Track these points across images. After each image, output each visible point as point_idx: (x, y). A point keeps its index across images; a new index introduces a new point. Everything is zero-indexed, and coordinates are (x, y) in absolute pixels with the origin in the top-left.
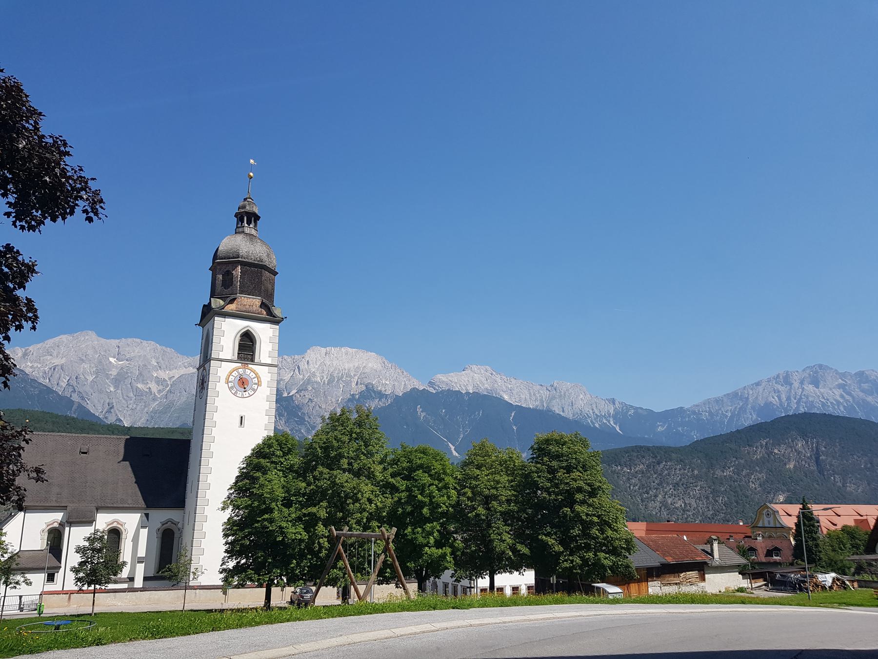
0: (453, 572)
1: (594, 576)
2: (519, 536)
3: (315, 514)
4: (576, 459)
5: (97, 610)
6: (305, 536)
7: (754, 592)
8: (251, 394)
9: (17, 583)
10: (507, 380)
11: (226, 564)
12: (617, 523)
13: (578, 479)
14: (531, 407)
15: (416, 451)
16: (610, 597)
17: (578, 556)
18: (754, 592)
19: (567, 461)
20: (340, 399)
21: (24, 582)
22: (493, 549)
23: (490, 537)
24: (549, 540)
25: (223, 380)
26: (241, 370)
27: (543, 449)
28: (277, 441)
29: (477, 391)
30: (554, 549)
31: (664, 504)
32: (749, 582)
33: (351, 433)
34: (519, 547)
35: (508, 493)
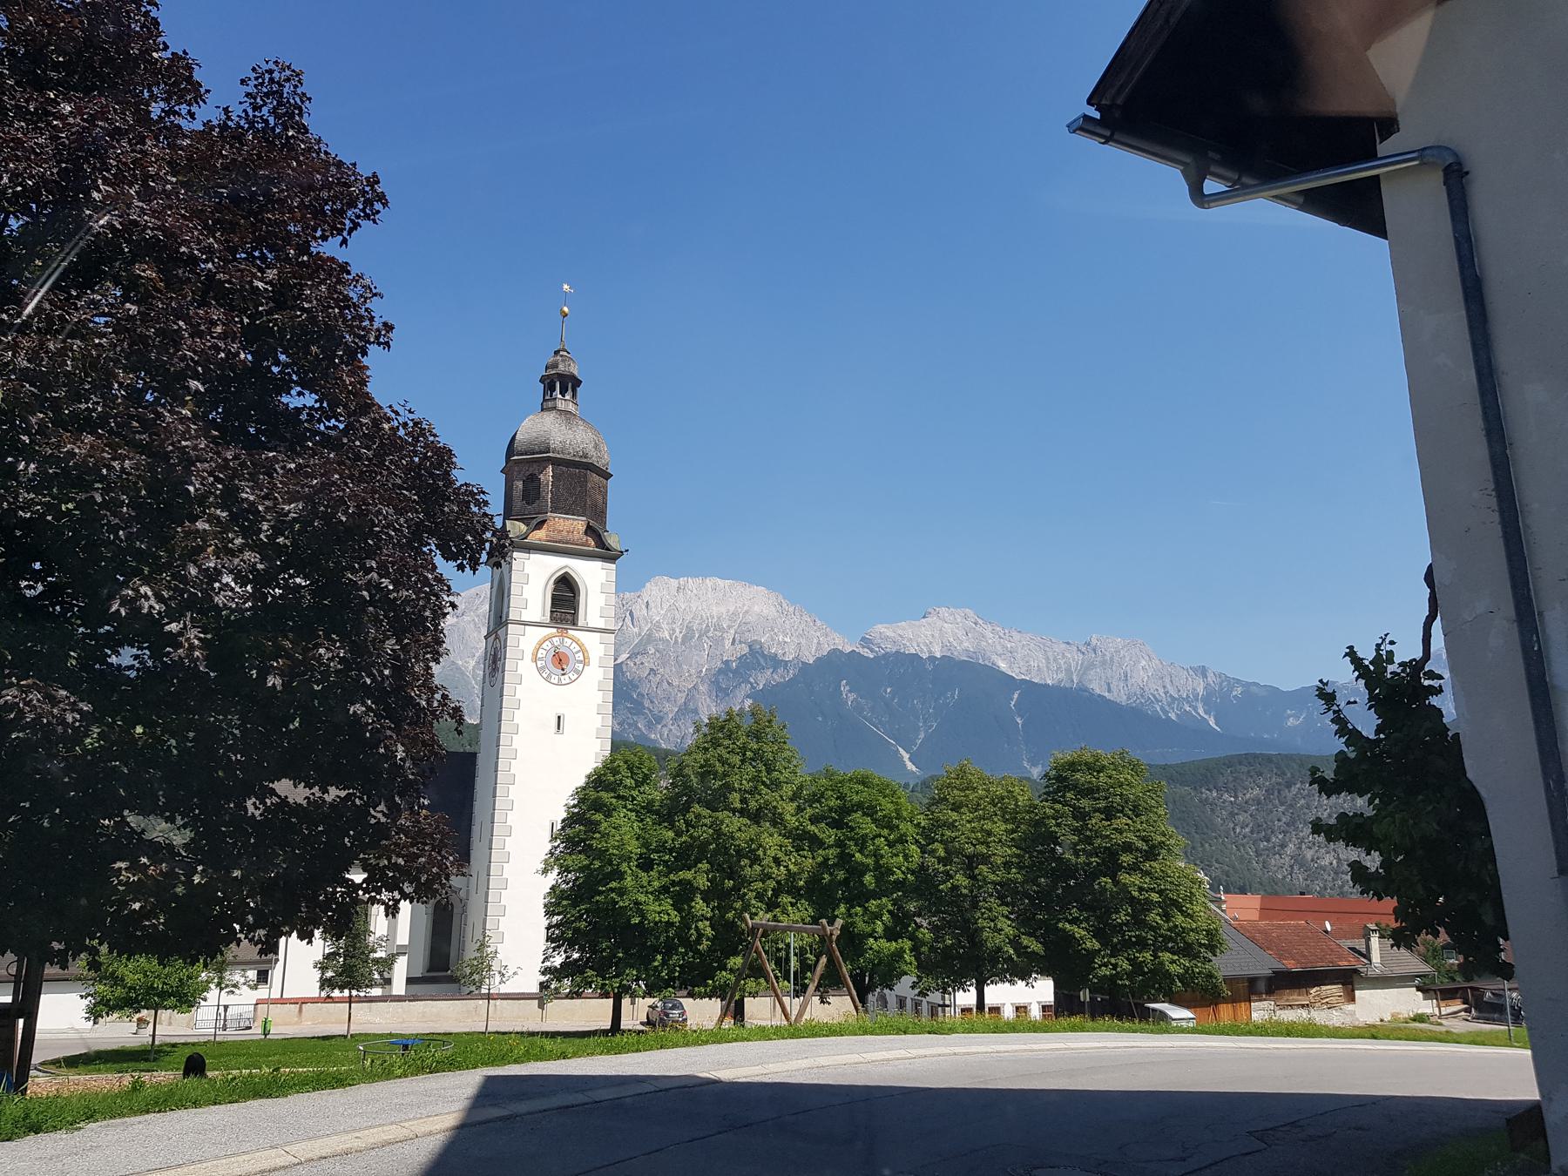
0: (915, 979)
1: (1153, 992)
2: (1025, 922)
3: (689, 882)
4: (1121, 795)
5: (354, 1029)
6: (675, 917)
7: (1443, 1022)
8: (573, 678)
9: (235, 986)
10: (1005, 634)
11: (551, 959)
12: (1192, 904)
13: (1124, 829)
14: (1050, 682)
15: (851, 780)
16: (1174, 1024)
17: (1125, 957)
18: (1443, 1022)
19: (1106, 798)
20: (704, 670)
21: (244, 984)
22: (982, 943)
23: (976, 923)
24: (1076, 930)
25: (528, 656)
26: (557, 639)
27: (1066, 779)
28: (626, 762)
29: (949, 654)
30: (1084, 946)
31: (1298, 860)
32: (1435, 1005)
33: (744, 749)
34: (1025, 941)
35: (1006, 851)
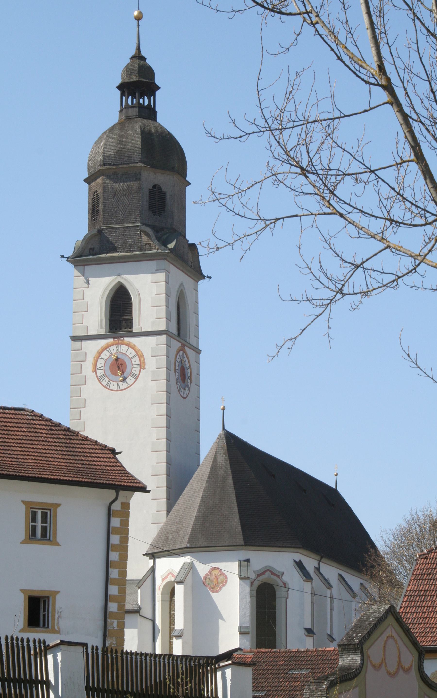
25: (90, 359)
